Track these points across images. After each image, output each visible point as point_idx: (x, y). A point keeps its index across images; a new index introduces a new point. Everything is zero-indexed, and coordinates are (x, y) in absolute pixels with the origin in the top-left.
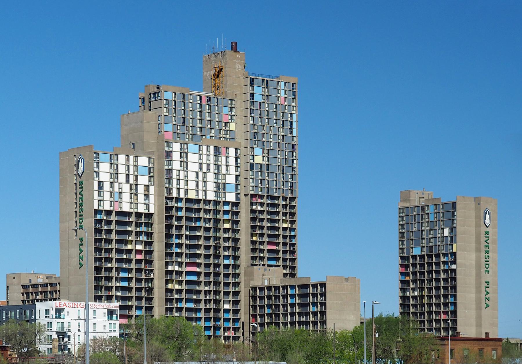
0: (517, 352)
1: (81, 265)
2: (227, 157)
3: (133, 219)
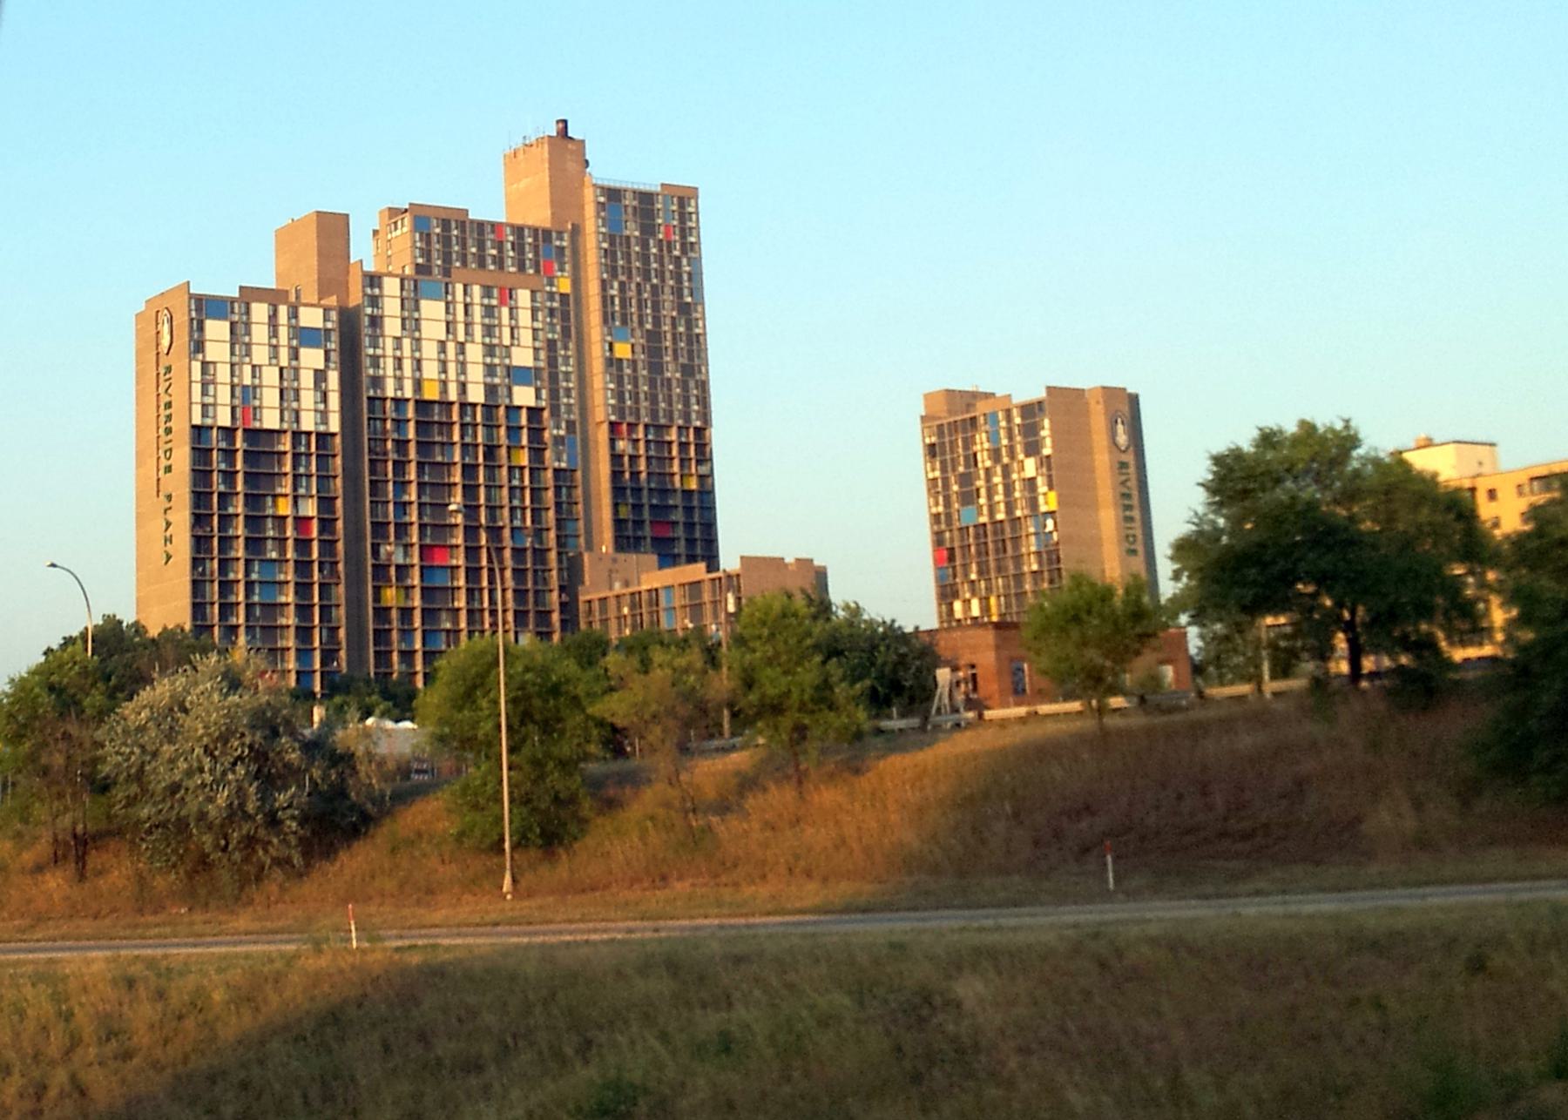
0: (859, 736)
1: (169, 557)
2: (511, 309)
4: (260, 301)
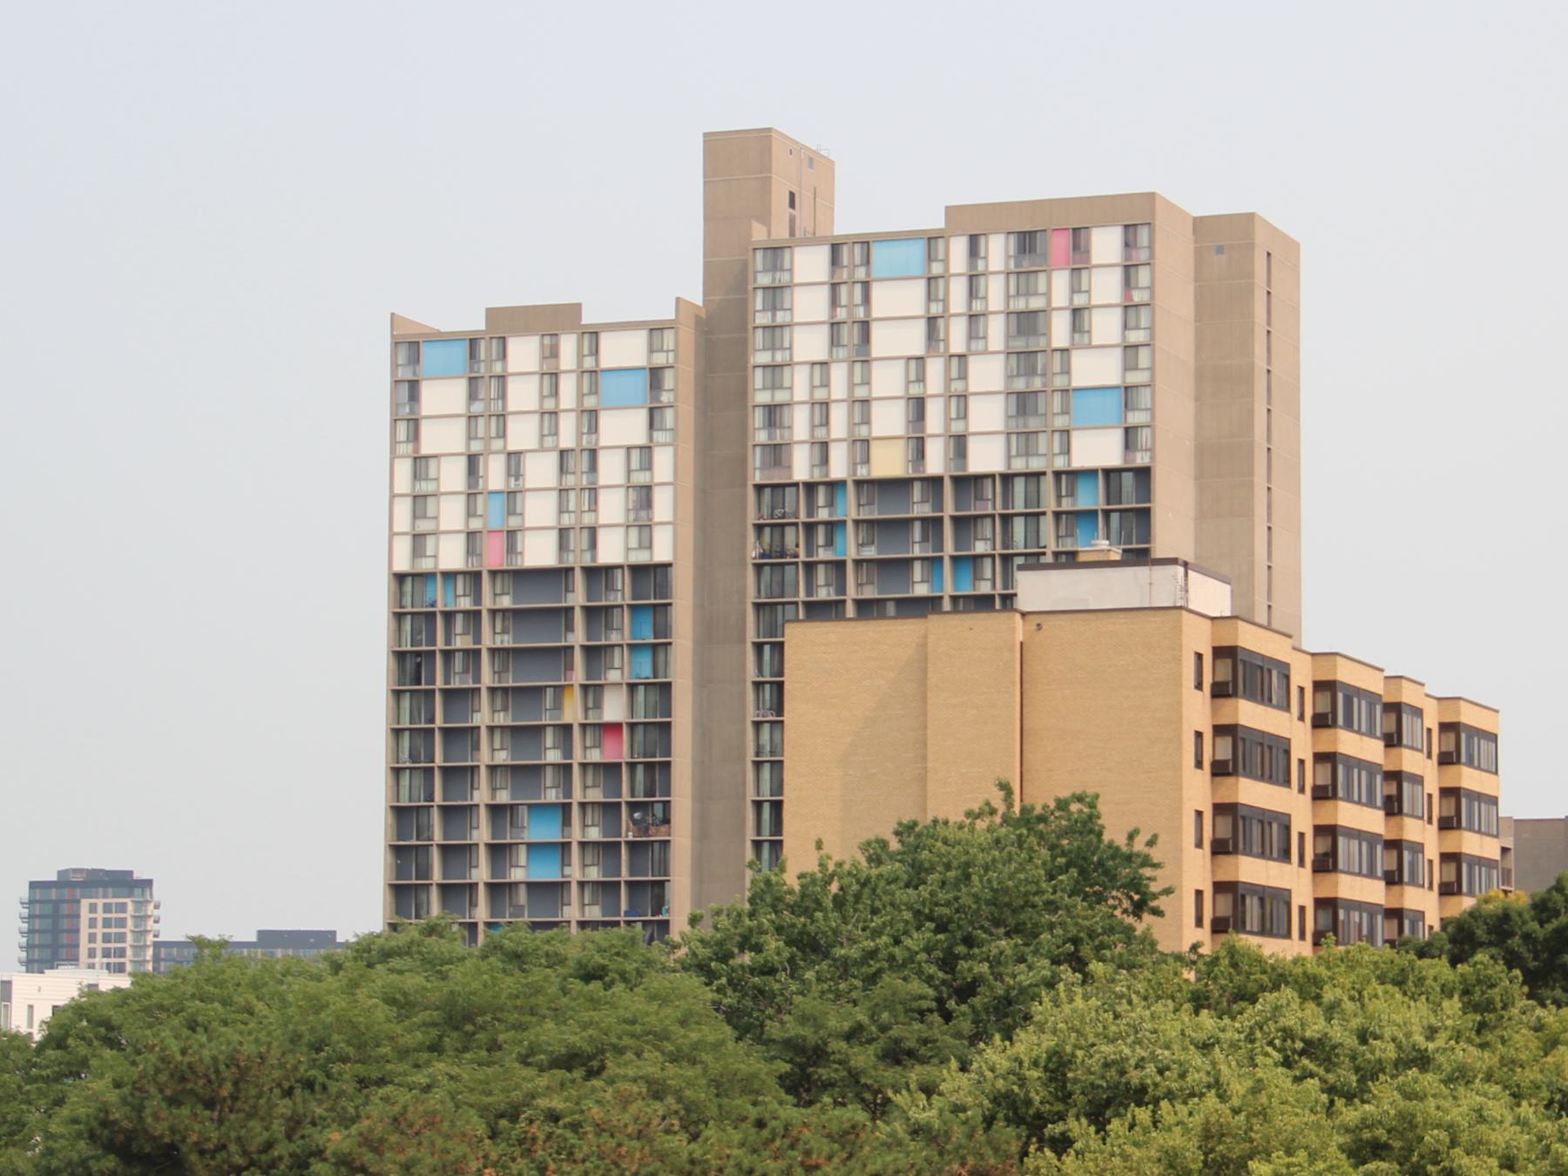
3: (578, 597)
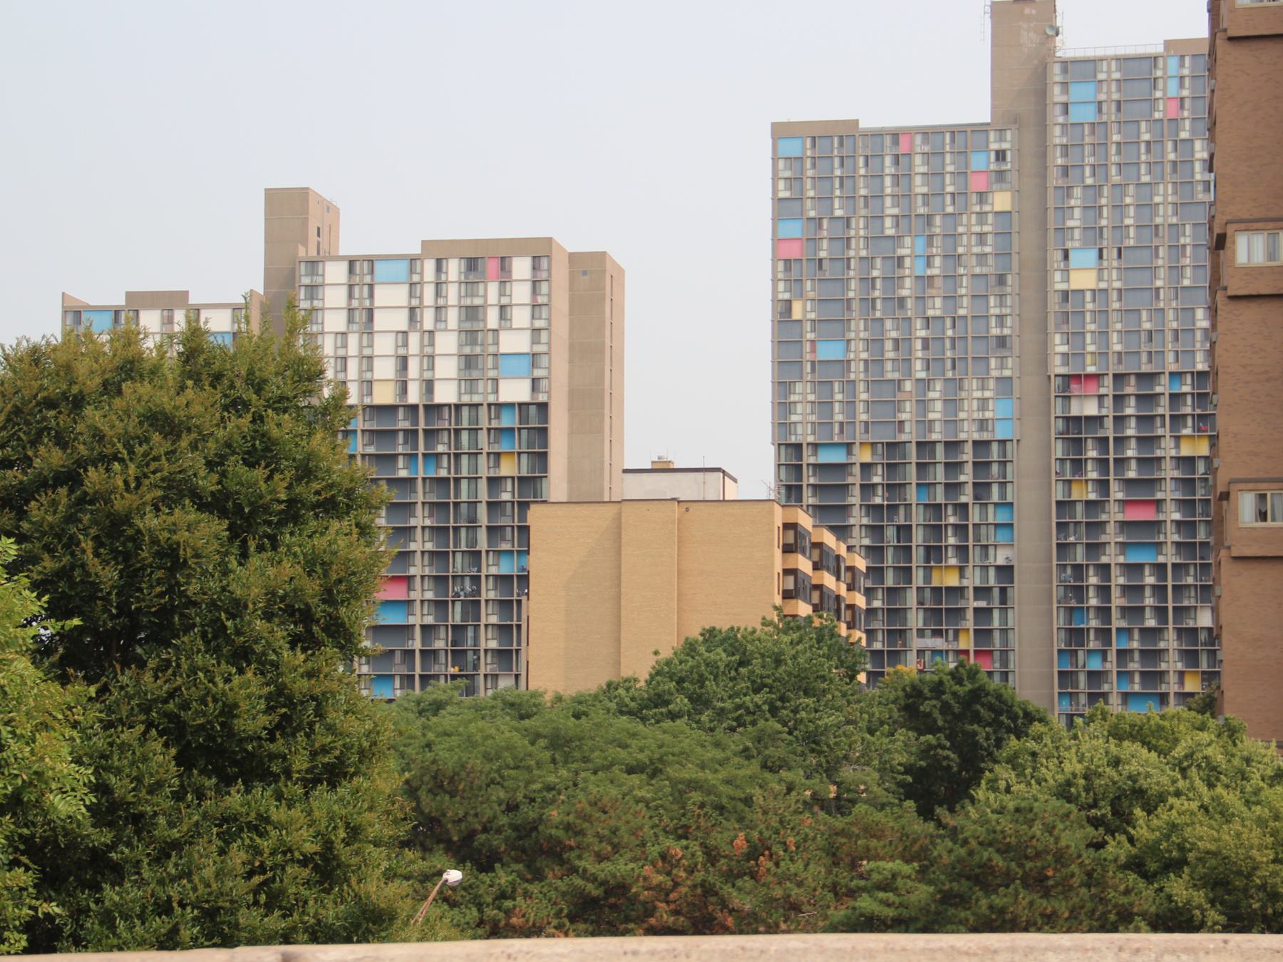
4: (151, 306)
